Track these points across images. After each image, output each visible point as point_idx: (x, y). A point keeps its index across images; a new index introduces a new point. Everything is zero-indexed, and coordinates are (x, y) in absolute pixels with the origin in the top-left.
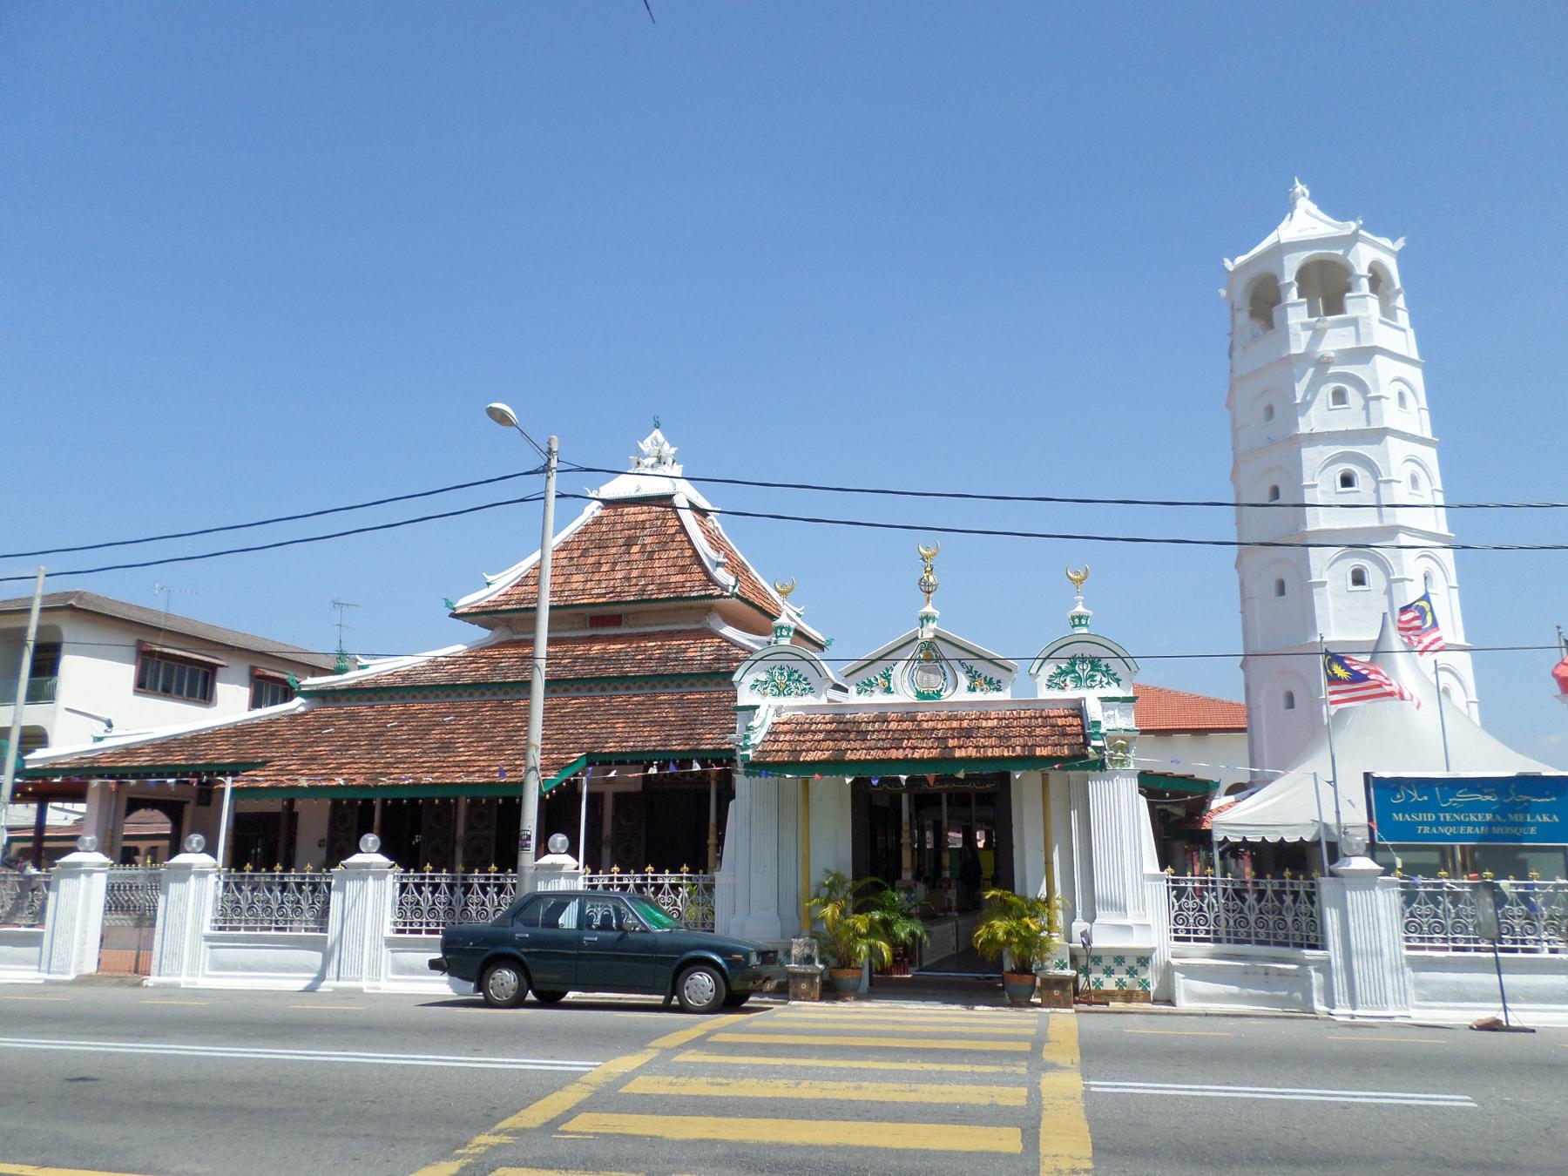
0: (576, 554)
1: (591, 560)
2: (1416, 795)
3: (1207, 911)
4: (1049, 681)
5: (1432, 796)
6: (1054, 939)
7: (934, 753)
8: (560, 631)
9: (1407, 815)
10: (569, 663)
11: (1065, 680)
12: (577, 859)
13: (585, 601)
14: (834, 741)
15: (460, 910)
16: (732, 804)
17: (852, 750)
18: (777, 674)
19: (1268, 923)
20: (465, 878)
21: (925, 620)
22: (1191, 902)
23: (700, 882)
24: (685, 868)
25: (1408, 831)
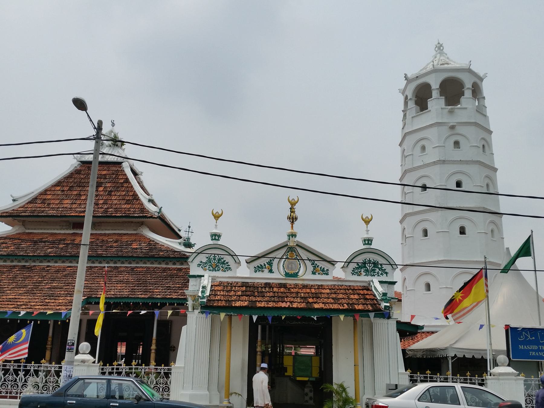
0: (66, 189)
1: (75, 193)
2: (529, 337)
3: (467, 395)
4: (353, 271)
5: (536, 337)
6: (358, 405)
7: (303, 305)
8: (54, 229)
9: (525, 346)
10: (63, 247)
11: (361, 271)
12: (95, 357)
13: (73, 214)
14: (247, 296)
15: (22, 384)
16: (184, 328)
17: (259, 302)
18: (212, 259)
19: (532, 401)
20: (25, 366)
21: (291, 237)
22: (162, 380)
23: (162, 371)
24: (468, 373)
25: (526, 353)
